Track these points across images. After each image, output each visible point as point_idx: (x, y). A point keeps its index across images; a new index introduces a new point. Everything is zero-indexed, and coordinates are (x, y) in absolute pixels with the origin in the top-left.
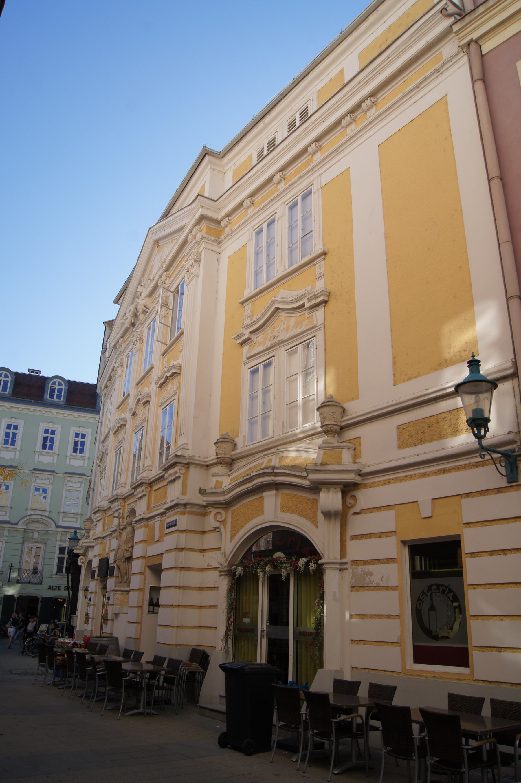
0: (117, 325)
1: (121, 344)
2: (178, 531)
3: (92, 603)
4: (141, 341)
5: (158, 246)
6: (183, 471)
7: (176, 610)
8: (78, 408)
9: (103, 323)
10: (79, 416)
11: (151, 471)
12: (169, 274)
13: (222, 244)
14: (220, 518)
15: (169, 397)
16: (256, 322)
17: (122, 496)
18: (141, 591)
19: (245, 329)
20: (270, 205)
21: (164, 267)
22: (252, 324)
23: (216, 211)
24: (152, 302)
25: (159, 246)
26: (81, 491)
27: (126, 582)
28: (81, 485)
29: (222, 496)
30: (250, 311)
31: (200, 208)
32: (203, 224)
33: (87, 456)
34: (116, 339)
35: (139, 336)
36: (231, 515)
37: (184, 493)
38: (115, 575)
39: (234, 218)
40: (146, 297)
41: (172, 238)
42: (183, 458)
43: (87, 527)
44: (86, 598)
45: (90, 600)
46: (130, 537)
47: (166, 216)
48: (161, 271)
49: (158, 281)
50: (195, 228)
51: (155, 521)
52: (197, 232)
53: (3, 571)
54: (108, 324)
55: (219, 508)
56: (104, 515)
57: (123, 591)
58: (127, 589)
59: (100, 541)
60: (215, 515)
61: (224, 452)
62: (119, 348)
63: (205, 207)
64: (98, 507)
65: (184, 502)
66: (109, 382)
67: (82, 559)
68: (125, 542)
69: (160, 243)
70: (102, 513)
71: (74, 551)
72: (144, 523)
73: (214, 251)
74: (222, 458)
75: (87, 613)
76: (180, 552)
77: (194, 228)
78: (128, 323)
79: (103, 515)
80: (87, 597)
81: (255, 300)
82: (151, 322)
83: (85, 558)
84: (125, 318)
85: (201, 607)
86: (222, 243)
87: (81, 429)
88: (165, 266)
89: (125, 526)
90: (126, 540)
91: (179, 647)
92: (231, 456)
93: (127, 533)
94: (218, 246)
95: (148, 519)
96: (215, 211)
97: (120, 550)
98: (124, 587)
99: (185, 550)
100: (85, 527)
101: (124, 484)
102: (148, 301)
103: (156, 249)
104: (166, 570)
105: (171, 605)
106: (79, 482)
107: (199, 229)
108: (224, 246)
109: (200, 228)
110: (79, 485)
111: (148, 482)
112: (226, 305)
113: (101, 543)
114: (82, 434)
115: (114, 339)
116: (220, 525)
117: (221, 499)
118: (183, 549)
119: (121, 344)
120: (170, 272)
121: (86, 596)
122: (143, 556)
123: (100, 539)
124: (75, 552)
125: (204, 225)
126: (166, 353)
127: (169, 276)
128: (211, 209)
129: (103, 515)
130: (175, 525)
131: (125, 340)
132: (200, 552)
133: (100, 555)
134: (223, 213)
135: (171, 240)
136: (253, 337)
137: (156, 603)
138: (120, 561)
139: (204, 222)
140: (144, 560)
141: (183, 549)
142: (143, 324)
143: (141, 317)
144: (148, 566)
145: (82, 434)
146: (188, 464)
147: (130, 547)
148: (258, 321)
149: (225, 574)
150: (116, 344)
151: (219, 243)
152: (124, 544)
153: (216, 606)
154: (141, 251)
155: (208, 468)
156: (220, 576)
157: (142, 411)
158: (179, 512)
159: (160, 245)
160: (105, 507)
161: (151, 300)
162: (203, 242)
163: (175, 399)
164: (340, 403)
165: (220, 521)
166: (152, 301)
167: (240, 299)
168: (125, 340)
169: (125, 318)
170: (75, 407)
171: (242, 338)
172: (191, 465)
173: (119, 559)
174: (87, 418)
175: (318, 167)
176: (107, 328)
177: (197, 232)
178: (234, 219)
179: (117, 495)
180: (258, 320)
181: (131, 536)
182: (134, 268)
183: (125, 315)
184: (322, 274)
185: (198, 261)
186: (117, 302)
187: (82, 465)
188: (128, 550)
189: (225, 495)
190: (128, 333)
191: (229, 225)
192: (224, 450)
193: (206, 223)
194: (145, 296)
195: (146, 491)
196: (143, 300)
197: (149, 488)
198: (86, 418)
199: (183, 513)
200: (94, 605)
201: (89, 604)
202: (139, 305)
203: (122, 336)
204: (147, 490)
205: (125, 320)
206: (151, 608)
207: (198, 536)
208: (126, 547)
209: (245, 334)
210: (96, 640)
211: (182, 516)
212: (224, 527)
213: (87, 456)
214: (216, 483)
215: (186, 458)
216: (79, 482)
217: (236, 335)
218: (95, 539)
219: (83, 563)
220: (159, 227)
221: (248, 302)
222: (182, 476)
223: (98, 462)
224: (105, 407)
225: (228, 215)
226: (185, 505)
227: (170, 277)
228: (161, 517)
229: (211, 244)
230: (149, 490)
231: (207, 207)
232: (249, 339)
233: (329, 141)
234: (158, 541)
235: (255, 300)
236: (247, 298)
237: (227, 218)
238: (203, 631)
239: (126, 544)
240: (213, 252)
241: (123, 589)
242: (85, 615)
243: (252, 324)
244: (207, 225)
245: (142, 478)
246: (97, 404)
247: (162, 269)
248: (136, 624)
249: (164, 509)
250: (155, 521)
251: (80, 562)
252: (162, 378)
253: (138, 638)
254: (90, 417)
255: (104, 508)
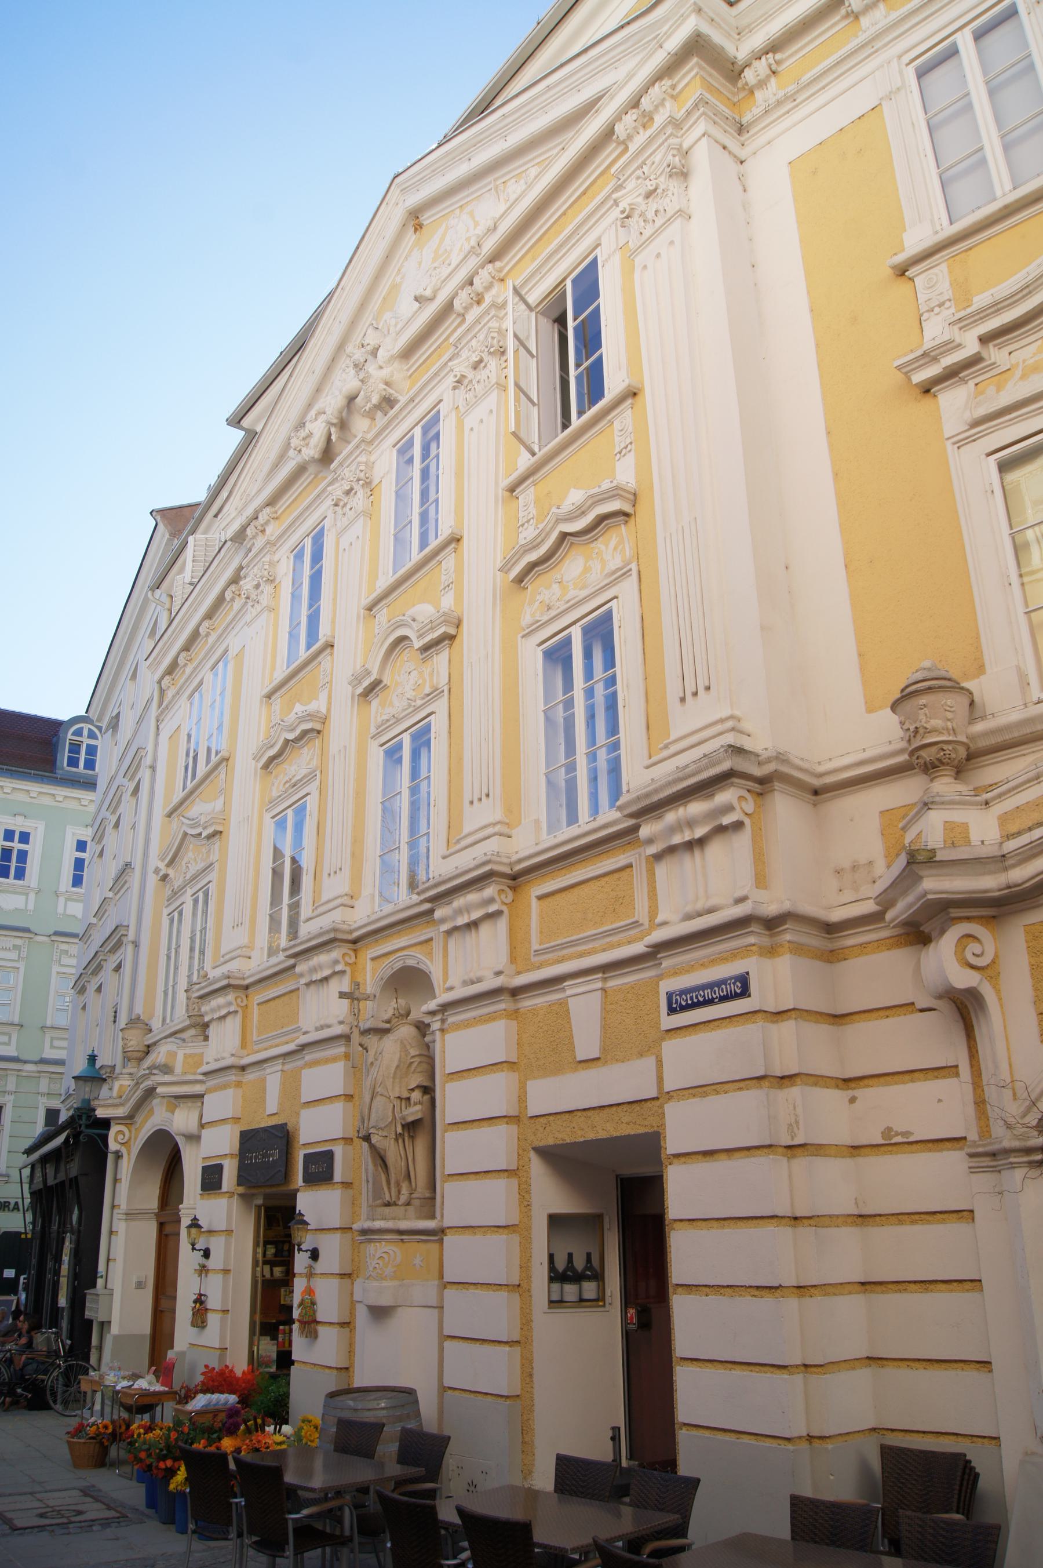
0: (250, 475)
1: (267, 523)
2: (760, 1015)
3: (213, 1263)
4: (368, 490)
5: (418, 227)
6: (749, 806)
7: (792, 1304)
8: (11, 770)
9: (151, 513)
10: (14, 788)
11: (510, 837)
12: (500, 270)
13: (748, 135)
14: (978, 956)
15: (581, 597)
16: (1020, 295)
17: (351, 932)
18: (514, 1231)
19: (960, 329)
20: (852, 63)
21: (316, 372)
22: (999, 306)
23: (732, 33)
24: (411, 376)
25: (421, 226)
26: (18, 968)
27: (408, 1204)
28: (19, 954)
29: (991, 873)
30: (947, 284)
31: (688, 16)
32: (691, 69)
33: (34, 884)
34: (249, 511)
35: (362, 475)
36: (1024, 945)
37: (761, 880)
38: (338, 1176)
39: (791, 58)
40: (392, 359)
41: (495, 180)
42: (753, 758)
43: (132, 1043)
44: (193, 1249)
45: (207, 1254)
46: (413, 1057)
47: (482, 112)
48: (473, 262)
49: (456, 294)
50: (657, 85)
51: (569, 992)
52: (664, 99)
53: (8, 1176)
54: (163, 517)
55: (968, 919)
56: (242, 1002)
57: (400, 1232)
58: (430, 1224)
59: (233, 1078)
60: (959, 939)
61: (949, 724)
62: (254, 537)
63: (705, 12)
64: (229, 977)
65: (771, 909)
66: (184, 654)
67: (120, 1132)
68: (395, 1073)
69: (426, 218)
70: (237, 994)
71: (97, 1113)
72: (502, 1006)
73: (730, 152)
74: (945, 747)
75: (201, 1295)
76: (778, 1091)
77: (653, 84)
78: (316, 446)
79: (239, 1000)
80: (197, 1247)
81: (970, 249)
82: (416, 425)
83: (130, 1131)
84: (303, 434)
85: (868, 1287)
86: (751, 133)
87: (19, 820)
88: (489, 245)
89: (388, 1022)
90: (398, 1067)
91: (830, 1446)
92: (972, 738)
93: (402, 1042)
94: (738, 140)
95: (515, 992)
96: (730, 35)
97: (379, 1101)
98: (405, 1219)
99: (798, 1080)
100: (125, 1044)
101: (346, 898)
102: (397, 372)
103: (410, 237)
104: (700, 1157)
105: (776, 1288)
106: (16, 947)
107: (669, 90)
108: (757, 140)
109: (673, 87)
110: (14, 955)
111: (507, 870)
112: (808, 293)
113: (239, 1084)
114: (21, 833)
115: (240, 513)
116: (981, 980)
117: (989, 883)
118: (786, 1080)
119: (267, 523)
120: (508, 263)
121: (193, 1245)
122: (512, 1113)
123: (234, 1071)
124: (100, 1113)
125: (693, 70)
126: (531, 480)
127: (502, 275)
128: (719, 24)
129: (239, 1000)
130: (745, 992)
131: (279, 512)
132: (837, 1087)
133: (236, 1120)
134: (758, 40)
135: (492, 186)
136: (996, 354)
137: (565, 1271)
138: (385, 1134)
139: (697, 63)
140: (514, 1128)
141: (786, 1080)
142: (371, 442)
143: (360, 426)
144: (537, 1150)
145: (21, 833)
146: (762, 781)
147: (413, 1090)
148: (1030, 292)
149: (1030, 1163)
150: (244, 529)
151: (741, 129)
152: (394, 1078)
153: (976, 1283)
154: (357, 248)
155: (819, 797)
156: (973, 1170)
157: (414, 674)
158: (753, 948)
159: (425, 223)
160: (249, 977)
161: (408, 370)
162: (704, 113)
163: (616, 597)
164: (959, 681)
165: (979, 965)
166: (411, 371)
167: (895, 254)
168: (279, 512)
169: (303, 434)
170: (5, 767)
171: (942, 360)
172: (777, 785)
173: (382, 1129)
174: (35, 796)
175: (831, 78)
176: (161, 526)
177: (664, 99)
178: (791, 61)
179: (335, 930)
180: (1031, 288)
181: (417, 1053)
182: (331, 295)
183: (301, 425)
184: (531, 516)
185: (683, 174)
186: (239, 422)
187: (23, 907)
188: (409, 1099)
189: (1006, 869)
190: (289, 495)
191: (773, 80)
192: (949, 715)
193: (701, 68)
194: (392, 356)
195: (503, 903)
196: (381, 368)
197: (510, 893)
198: (31, 795)
199: (771, 952)
200: (226, 1271)
201: (204, 1266)
202: (372, 380)
203: (271, 502)
204: (503, 896)
205: (304, 439)
206: (556, 1286)
207: (823, 1030)
208: (400, 1087)
209: (960, 345)
210: (356, 1410)
211: (767, 963)
212: (994, 987)
213: (34, 884)
214: (945, 829)
215: (760, 758)
216: (16, 947)
217: (919, 353)
218: (205, 1074)
219: (122, 1144)
220: (447, 154)
221: (934, 258)
222: (747, 821)
223: (162, 865)
224: (161, 727)
225: (774, 47)
226: (772, 924)
227: (502, 280)
228: (605, 980)
229: (721, 127)
230: (509, 900)
231: (713, 16)
232: (975, 360)
233: (817, 43)
234: (598, 1059)
235: (970, 249)
236: (937, 244)
237: (770, 55)
238: (891, 1372)
239: (397, 1080)
240: (726, 153)
241: (404, 1225)
242: (195, 1302)
243: (999, 306)
244: (702, 73)
245: (494, 858)
246: (58, 763)
247: (478, 255)
248: (507, 1348)
249: (647, 947)
250: (569, 992)
251: (116, 1140)
252: (536, 547)
253: (518, 1396)
254: (40, 793)
255: (244, 979)
